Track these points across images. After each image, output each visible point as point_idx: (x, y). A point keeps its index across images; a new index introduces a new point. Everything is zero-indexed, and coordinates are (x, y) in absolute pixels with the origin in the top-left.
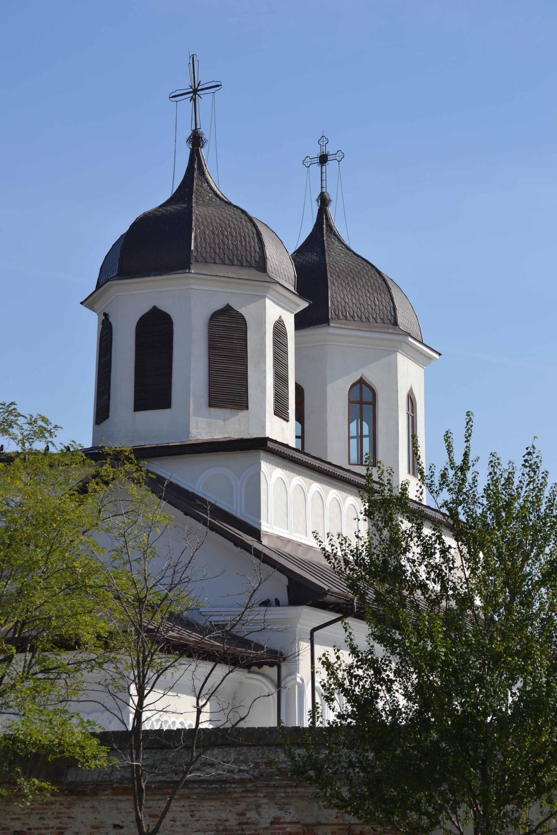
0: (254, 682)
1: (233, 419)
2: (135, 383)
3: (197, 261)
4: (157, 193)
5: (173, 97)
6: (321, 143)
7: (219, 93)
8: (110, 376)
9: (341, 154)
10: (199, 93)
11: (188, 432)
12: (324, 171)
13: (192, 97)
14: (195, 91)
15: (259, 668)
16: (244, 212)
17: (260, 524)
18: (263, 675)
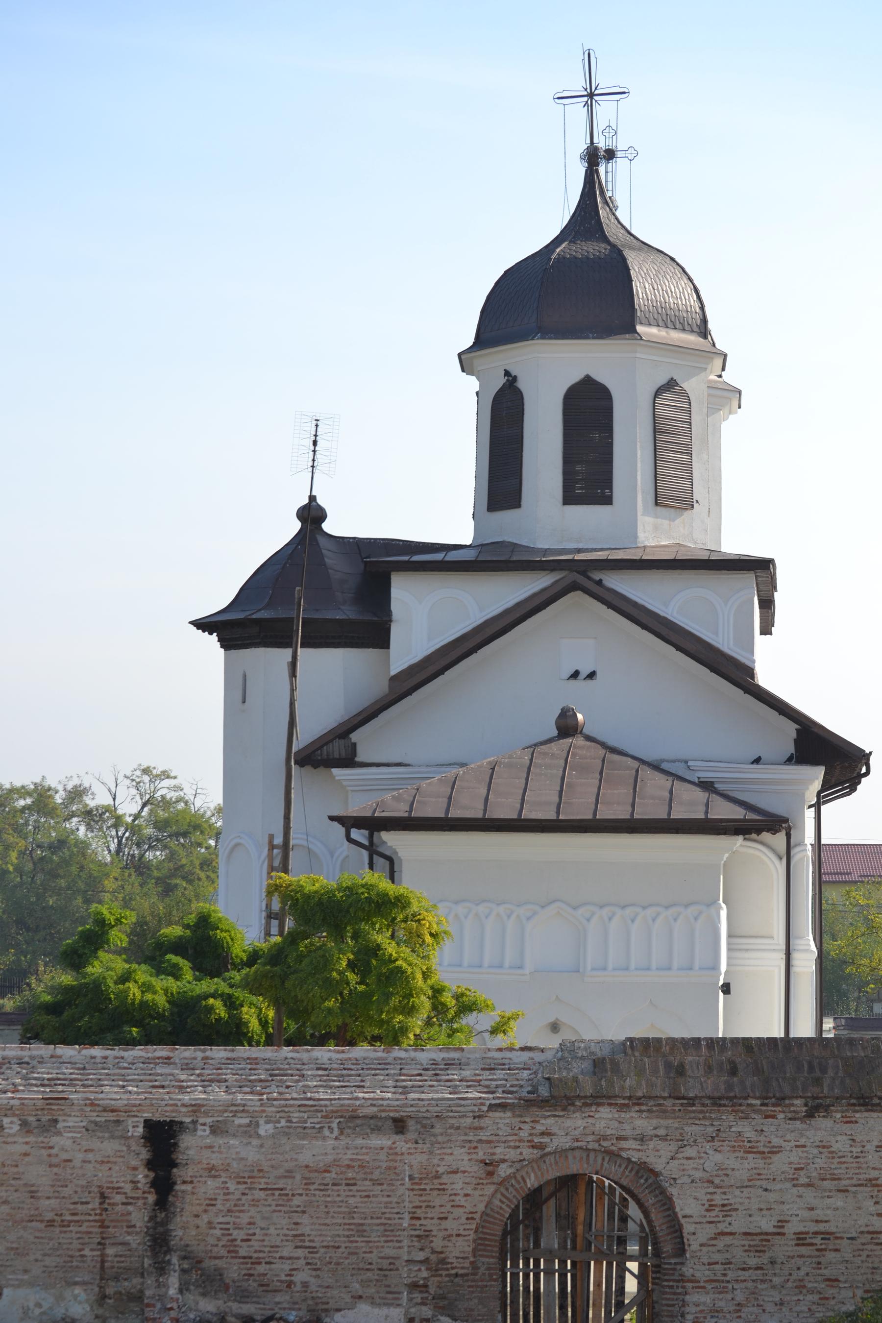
0: (751, 851)
1: (678, 521)
3: (641, 323)
4: (538, 222)
5: (559, 98)
6: (607, 135)
8: (522, 456)
9: (633, 152)
10: (596, 98)
12: (610, 169)
13: (587, 102)
14: (591, 95)
16: (672, 259)
17: (754, 662)
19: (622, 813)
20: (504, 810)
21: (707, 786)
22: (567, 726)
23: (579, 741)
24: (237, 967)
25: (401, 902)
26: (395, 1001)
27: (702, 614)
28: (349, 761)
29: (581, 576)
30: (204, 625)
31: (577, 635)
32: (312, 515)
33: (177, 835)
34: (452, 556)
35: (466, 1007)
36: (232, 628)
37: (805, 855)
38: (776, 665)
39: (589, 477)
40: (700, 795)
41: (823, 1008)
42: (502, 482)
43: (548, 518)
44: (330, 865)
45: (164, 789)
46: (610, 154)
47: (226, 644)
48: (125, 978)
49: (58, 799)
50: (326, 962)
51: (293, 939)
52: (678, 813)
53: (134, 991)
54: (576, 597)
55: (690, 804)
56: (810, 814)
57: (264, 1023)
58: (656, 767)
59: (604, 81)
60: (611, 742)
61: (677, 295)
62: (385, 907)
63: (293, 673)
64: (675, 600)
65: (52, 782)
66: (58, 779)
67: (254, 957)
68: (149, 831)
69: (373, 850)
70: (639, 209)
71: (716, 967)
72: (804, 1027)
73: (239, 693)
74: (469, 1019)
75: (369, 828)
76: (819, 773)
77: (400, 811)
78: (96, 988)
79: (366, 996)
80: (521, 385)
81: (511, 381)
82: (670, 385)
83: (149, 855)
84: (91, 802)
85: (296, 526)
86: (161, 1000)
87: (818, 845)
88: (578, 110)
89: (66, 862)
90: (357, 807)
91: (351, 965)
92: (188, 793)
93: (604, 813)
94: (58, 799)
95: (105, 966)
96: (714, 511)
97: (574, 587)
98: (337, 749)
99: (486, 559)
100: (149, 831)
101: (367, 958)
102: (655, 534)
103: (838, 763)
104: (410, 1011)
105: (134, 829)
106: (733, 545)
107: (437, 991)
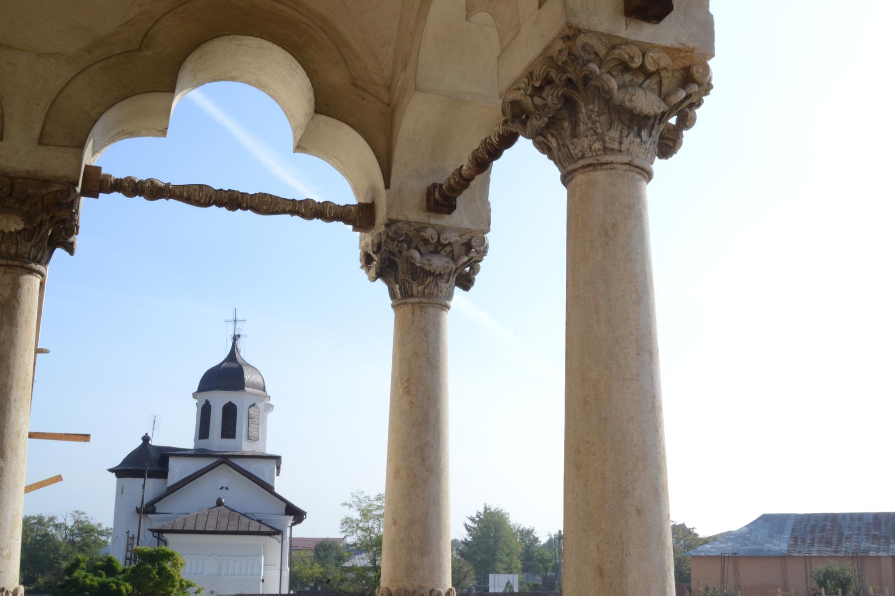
4: (217, 357)
19: (235, 529)
20: (200, 528)
21: (259, 521)
22: (219, 503)
23: (223, 507)
24: (120, 574)
25: (172, 555)
26: (169, 583)
27: (257, 470)
28: (153, 512)
29: (225, 460)
30: (111, 470)
31: (223, 477)
32: (146, 439)
33: (86, 533)
34: (188, 452)
35: (189, 586)
36: (121, 472)
37: (287, 542)
38: (281, 486)
39: (229, 430)
40: (258, 524)
41: (291, 588)
42: (203, 431)
43: (216, 442)
44: (148, 544)
45: (82, 518)
46: (239, 336)
47: (118, 476)
48: (85, 577)
49: (46, 520)
50: (149, 572)
51: (139, 565)
52: (251, 529)
53: (88, 581)
54: (223, 465)
55: (255, 526)
56: (289, 529)
57: (127, 591)
58: (245, 515)
59: (239, 317)
60: (232, 507)
61: (258, 380)
62: (168, 556)
63: (144, 488)
64: (252, 467)
65: (44, 515)
66: (46, 514)
67: (124, 571)
68: (77, 531)
69: (159, 539)
70: (246, 354)
71: (260, 574)
72: (285, 591)
73: (120, 491)
74: (188, 590)
75: (159, 533)
76: (292, 517)
77: (169, 527)
78: (76, 581)
79: (161, 582)
80: (211, 403)
81: (207, 402)
82: (254, 405)
83: (76, 539)
84: (57, 522)
85: (141, 442)
86: (96, 584)
87: (291, 538)
88: (231, 325)
89: (48, 541)
90: (156, 526)
91: (157, 573)
92: (89, 520)
93: (230, 529)
94: (46, 520)
95: (78, 574)
96: (264, 441)
97: (223, 462)
98: (150, 508)
99: (198, 453)
100: (77, 531)
101: (162, 571)
102: (247, 448)
103: (298, 515)
104: (173, 586)
105: (71, 531)
106: (269, 451)
107: (181, 581)
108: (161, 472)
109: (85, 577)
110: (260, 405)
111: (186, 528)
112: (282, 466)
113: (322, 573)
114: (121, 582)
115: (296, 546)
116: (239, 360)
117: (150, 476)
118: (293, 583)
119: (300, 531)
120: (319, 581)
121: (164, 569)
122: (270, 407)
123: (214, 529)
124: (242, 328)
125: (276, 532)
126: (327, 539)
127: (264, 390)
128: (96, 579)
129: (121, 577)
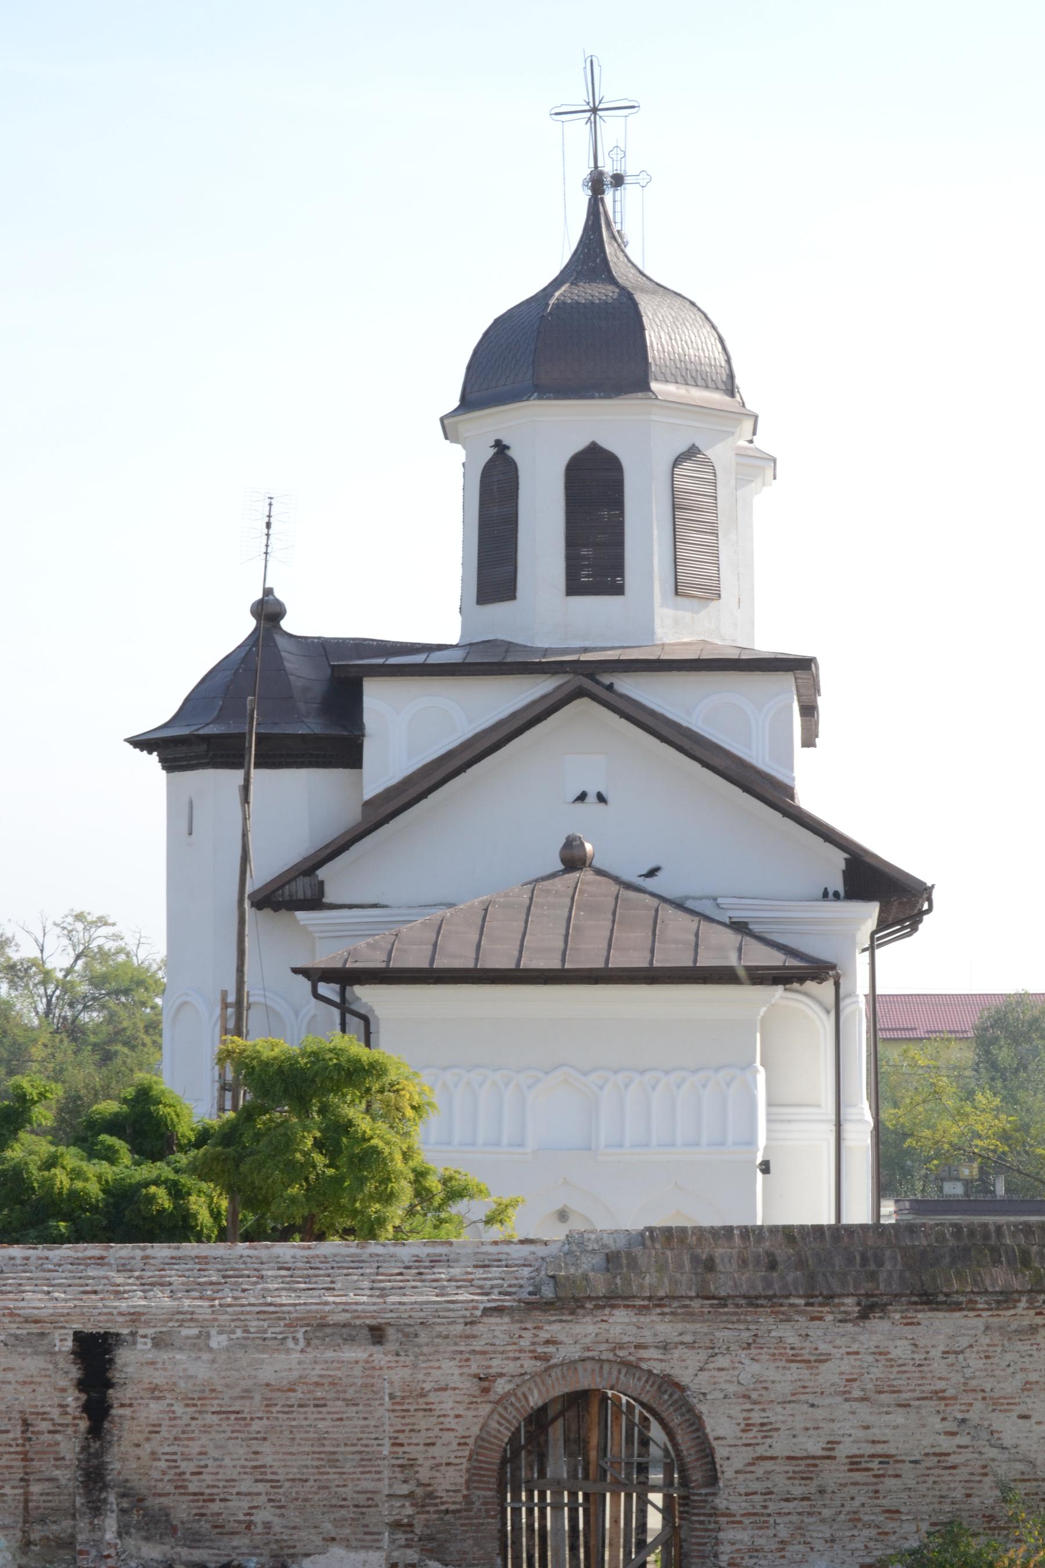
0: (809, 1012)
2: (480, 522)
3: (656, 380)
4: (531, 263)
5: (556, 114)
7: (634, 117)
11: (652, 632)
12: (618, 198)
14: (594, 110)
15: (801, 984)
18: (806, 994)
19: (638, 960)
20: (500, 959)
21: (740, 927)
22: (573, 859)
23: (586, 875)
24: (183, 1149)
26: (370, 1187)
27: (720, 727)
28: (315, 902)
29: (588, 681)
30: (142, 743)
31: (584, 749)
32: (268, 612)
34: (436, 658)
35: (455, 1193)
36: (177, 748)
37: (857, 1009)
38: (819, 784)
39: (596, 561)
40: (731, 938)
41: (881, 1189)
42: (494, 572)
43: (548, 613)
44: (293, 1027)
45: (101, 938)
46: (618, 180)
47: (170, 765)
48: (51, 1163)
50: (287, 1142)
52: (707, 960)
53: (61, 1179)
54: (583, 704)
56: (862, 960)
58: (679, 905)
59: (609, 93)
61: (698, 345)
67: (204, 1136)
68: (84, 988)
69: (344, 1007)
70: (651, 244)
71: (751, 1142)
72: (859, 1212)
73: (184, 823)
74: (457, 1208)
76: (873, 909)
77: (376, 961)
79: (338, 1180)
81: (501, 447)
82: (691, 453)
83: (85, 1017)
85: (249, 624)
86: (93, 1188)
87: (873, 997)
90: (326, 957)
91: (318, 1145)
97: (580, 693)
98: (301, 888)
99: (481, 661)
100: (84, 988)
101: (336, 1136)
102: (675, 629)
103: (893, 897)
104: (388, 1198)
105: (65, 986)
107: (420, 1175)
108: (342, 749)
109: (51, 1163)
110: (719, 453)
111: (442, 962)
112: (822, 702)
113: (1005, 1137)
114: (186, 1180)
115: (895, 1025)
116: (619, 268)
117: (265, 761)
118: (892, 1166)
119: (909, 967)
120: (992, 1164)
121: (346, 1127)
122: (761, 465)
123: (510, 964)
124: (623, 142)
125: (807, 971)
126: (1021, 999)
127: (730, 388)
128: (95, 1169)
129: (183, 1159)
